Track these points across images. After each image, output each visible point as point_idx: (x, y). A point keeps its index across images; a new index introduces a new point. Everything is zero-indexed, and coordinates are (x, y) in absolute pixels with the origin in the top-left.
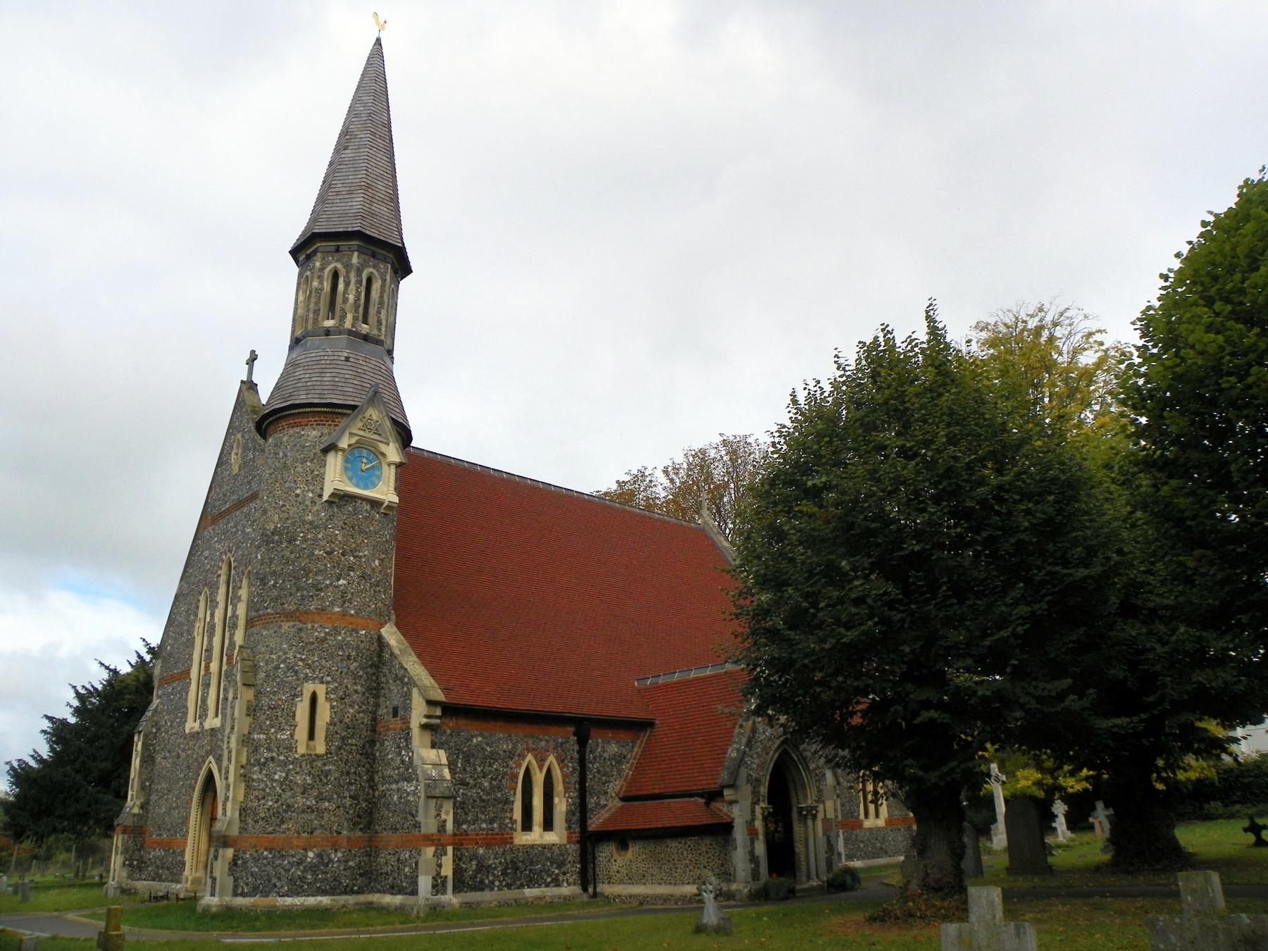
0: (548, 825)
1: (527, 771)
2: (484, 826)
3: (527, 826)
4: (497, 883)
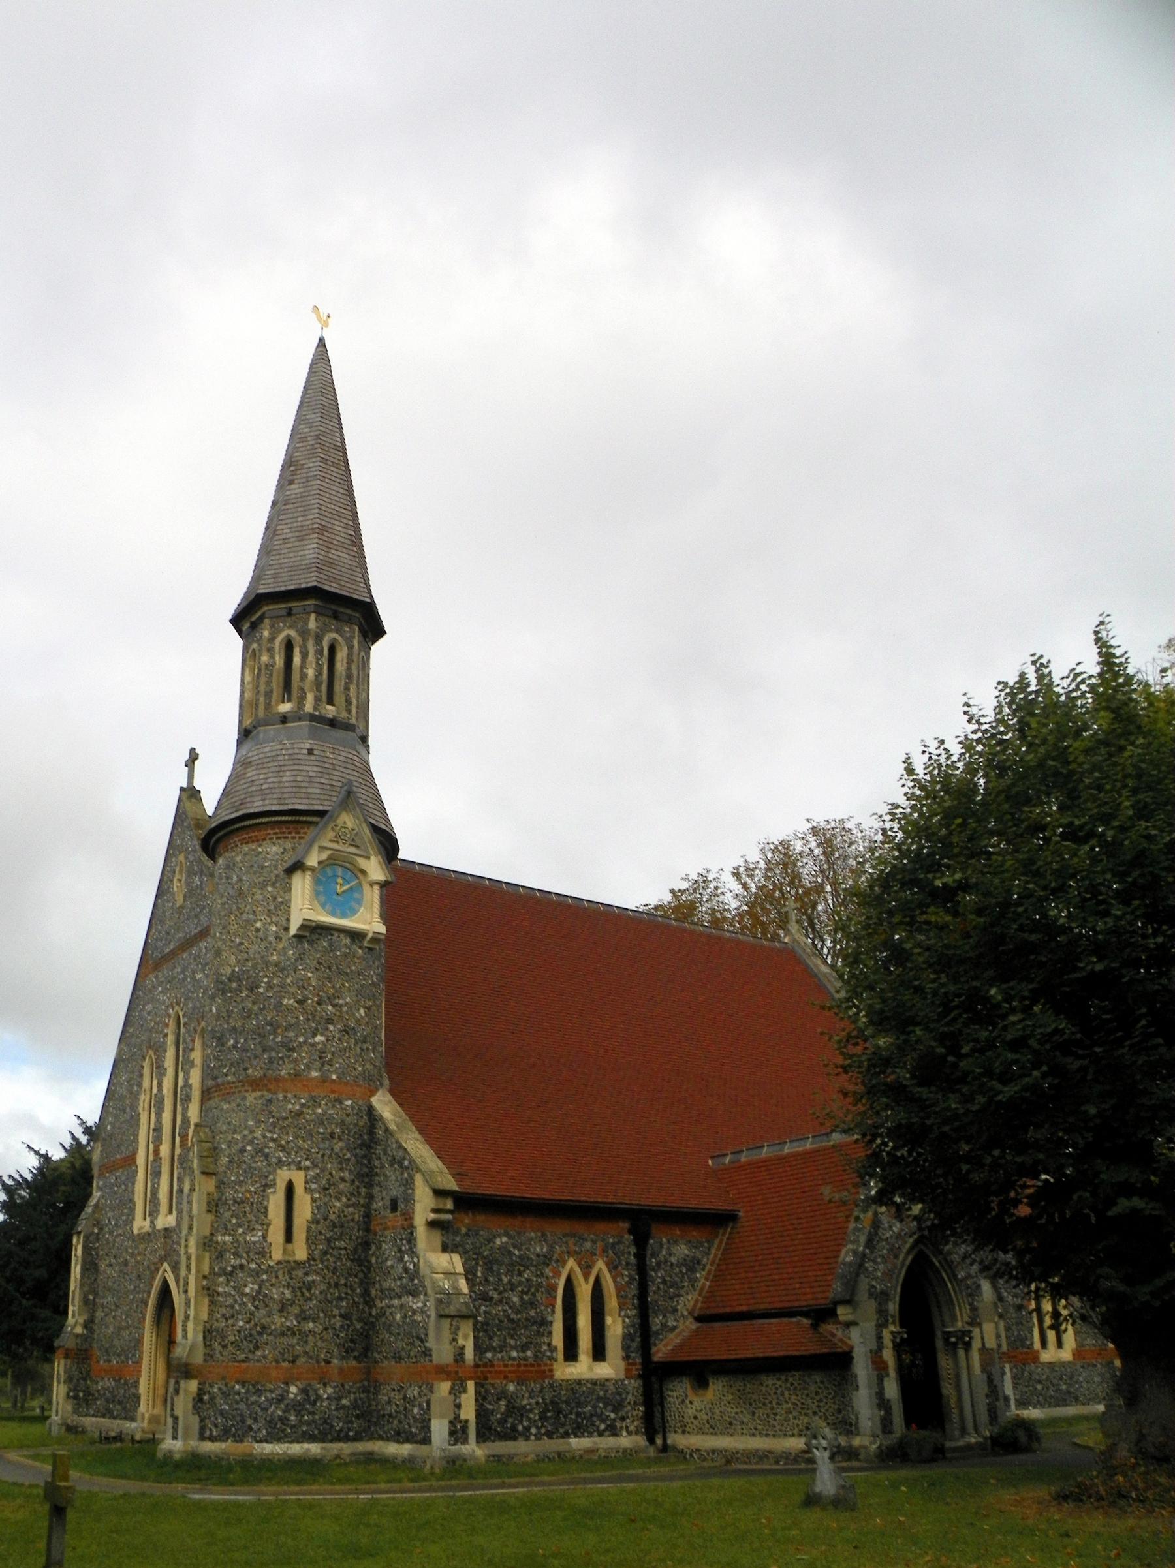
0: (599, 1353)
2: (514, 1354)
3: (571, 1354)
4: (533, 1430)
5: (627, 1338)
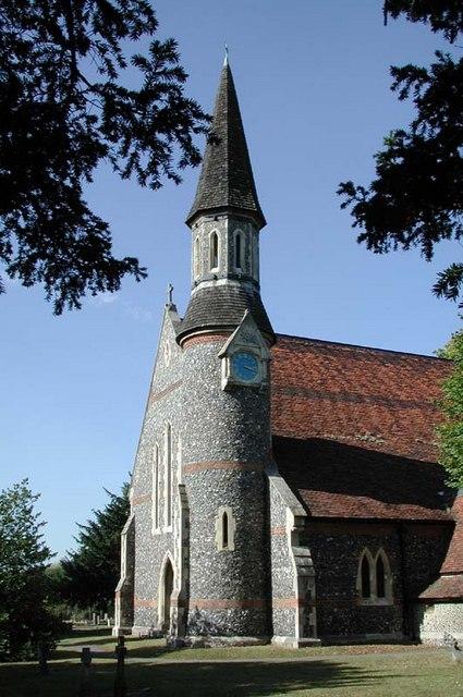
0: (381, 594)
1: (365, 557)
3: (366, 593)
5: (395, 586)
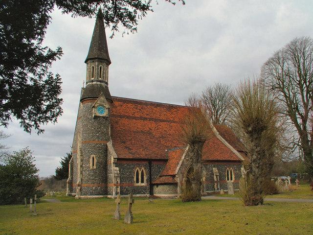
0: (142, 182)
1: (137, 171)
3: (137, 182)
